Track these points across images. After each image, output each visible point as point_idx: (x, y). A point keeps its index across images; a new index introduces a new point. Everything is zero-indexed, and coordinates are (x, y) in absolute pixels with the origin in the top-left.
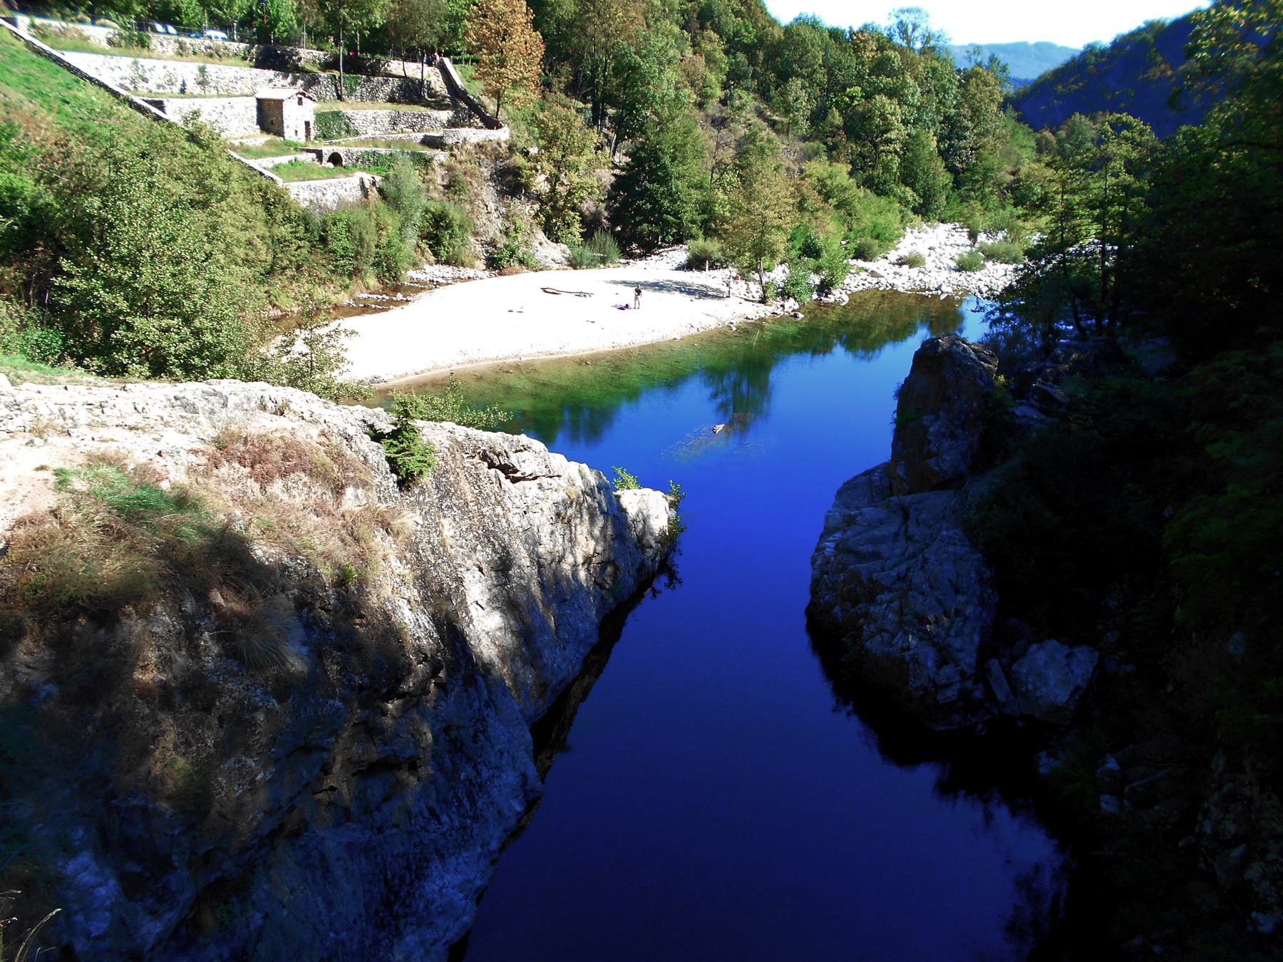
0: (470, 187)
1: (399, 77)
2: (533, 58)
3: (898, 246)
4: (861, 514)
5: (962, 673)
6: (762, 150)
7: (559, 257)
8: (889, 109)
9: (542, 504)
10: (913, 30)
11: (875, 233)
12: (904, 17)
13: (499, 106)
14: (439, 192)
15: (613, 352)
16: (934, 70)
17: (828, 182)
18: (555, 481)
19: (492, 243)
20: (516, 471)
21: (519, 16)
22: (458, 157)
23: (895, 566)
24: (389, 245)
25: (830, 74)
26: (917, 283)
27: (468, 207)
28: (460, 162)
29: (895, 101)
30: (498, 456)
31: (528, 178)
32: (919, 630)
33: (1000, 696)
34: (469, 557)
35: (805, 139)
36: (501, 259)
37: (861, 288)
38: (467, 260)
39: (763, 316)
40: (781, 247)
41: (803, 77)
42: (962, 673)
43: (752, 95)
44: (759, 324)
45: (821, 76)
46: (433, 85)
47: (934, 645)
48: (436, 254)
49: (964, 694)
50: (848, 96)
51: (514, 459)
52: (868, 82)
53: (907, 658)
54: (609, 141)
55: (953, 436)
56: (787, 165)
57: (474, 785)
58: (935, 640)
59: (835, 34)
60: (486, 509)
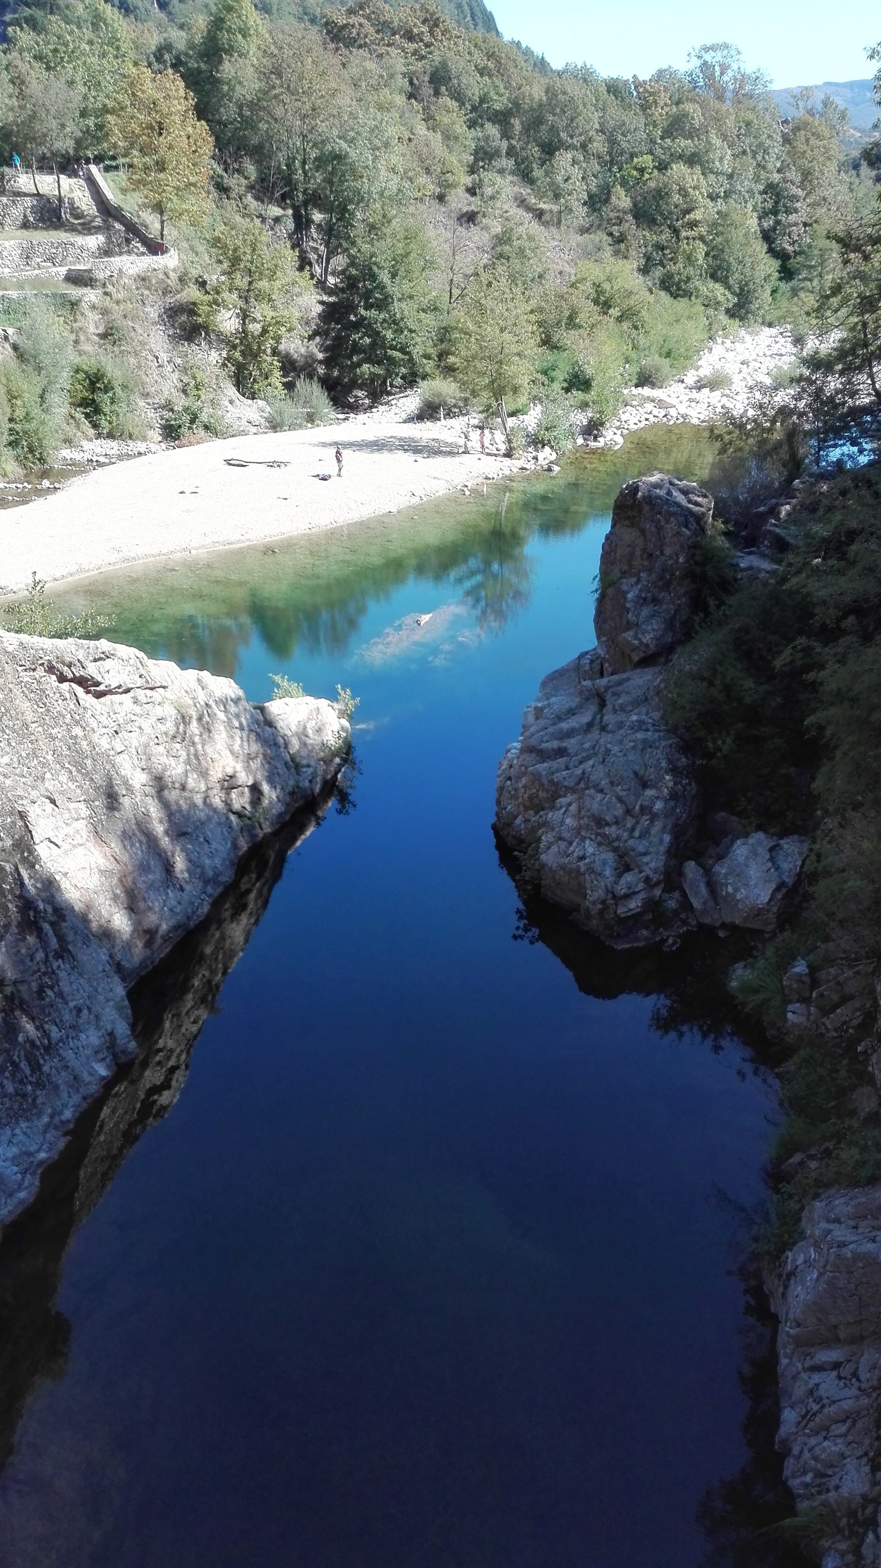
0: (133, 334)
1: (34, 195)
2: (199, 156)
3: (700, 363)
4: (549, 705)
5: (647, 879)
6: (522, 250)
7: (256, 417)
8: (690, 182)
9: (140, 721)
10: (722, 74)
11: (665, 350)
12: (708, 57)
13: (162, 222)
14: (94, 344)
15: (309, 535)
16: (748, 124)
17: (606, 286)
18: (157, 695)
19: (168, 406)
20: (98, 684)
21: (175, 102)
22: (115, 296)
23: (581, 763)
24: (28, 417)
25: (612, 142)
26: (719, 410)
27: (132, 360)
28: (118, 302)
29: (698, 169)
30: (69, 666)
31: (208, 315)
32: (597, 834)
33: (696, 904)
34: (34, 788)
35: (583, 231)
36: (180, 427)
37: (642, 425)
38: (136, 432)
39: (508, 473)
40: (524, 381)
41: (575, 148)
42: (647, 879)
43: (510, 178)
44: (505, 486)
45: (599, 145)
46: (77, 204)
47: (615, 850)
48: (95, 426)
49: (653, 906)
50: (636, 169)
51: (92, 670)
52: (662, 148)
53: (583, 869)
54: (320, 256)
55: (655, 601)
56: (560, 268)
57: (38, 1048)
58: (616, 844)
59: (614, 88)
60: (56, 730)
